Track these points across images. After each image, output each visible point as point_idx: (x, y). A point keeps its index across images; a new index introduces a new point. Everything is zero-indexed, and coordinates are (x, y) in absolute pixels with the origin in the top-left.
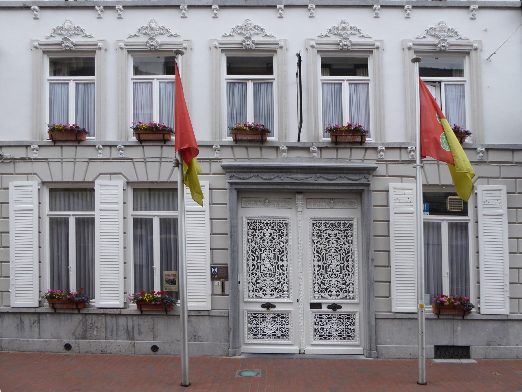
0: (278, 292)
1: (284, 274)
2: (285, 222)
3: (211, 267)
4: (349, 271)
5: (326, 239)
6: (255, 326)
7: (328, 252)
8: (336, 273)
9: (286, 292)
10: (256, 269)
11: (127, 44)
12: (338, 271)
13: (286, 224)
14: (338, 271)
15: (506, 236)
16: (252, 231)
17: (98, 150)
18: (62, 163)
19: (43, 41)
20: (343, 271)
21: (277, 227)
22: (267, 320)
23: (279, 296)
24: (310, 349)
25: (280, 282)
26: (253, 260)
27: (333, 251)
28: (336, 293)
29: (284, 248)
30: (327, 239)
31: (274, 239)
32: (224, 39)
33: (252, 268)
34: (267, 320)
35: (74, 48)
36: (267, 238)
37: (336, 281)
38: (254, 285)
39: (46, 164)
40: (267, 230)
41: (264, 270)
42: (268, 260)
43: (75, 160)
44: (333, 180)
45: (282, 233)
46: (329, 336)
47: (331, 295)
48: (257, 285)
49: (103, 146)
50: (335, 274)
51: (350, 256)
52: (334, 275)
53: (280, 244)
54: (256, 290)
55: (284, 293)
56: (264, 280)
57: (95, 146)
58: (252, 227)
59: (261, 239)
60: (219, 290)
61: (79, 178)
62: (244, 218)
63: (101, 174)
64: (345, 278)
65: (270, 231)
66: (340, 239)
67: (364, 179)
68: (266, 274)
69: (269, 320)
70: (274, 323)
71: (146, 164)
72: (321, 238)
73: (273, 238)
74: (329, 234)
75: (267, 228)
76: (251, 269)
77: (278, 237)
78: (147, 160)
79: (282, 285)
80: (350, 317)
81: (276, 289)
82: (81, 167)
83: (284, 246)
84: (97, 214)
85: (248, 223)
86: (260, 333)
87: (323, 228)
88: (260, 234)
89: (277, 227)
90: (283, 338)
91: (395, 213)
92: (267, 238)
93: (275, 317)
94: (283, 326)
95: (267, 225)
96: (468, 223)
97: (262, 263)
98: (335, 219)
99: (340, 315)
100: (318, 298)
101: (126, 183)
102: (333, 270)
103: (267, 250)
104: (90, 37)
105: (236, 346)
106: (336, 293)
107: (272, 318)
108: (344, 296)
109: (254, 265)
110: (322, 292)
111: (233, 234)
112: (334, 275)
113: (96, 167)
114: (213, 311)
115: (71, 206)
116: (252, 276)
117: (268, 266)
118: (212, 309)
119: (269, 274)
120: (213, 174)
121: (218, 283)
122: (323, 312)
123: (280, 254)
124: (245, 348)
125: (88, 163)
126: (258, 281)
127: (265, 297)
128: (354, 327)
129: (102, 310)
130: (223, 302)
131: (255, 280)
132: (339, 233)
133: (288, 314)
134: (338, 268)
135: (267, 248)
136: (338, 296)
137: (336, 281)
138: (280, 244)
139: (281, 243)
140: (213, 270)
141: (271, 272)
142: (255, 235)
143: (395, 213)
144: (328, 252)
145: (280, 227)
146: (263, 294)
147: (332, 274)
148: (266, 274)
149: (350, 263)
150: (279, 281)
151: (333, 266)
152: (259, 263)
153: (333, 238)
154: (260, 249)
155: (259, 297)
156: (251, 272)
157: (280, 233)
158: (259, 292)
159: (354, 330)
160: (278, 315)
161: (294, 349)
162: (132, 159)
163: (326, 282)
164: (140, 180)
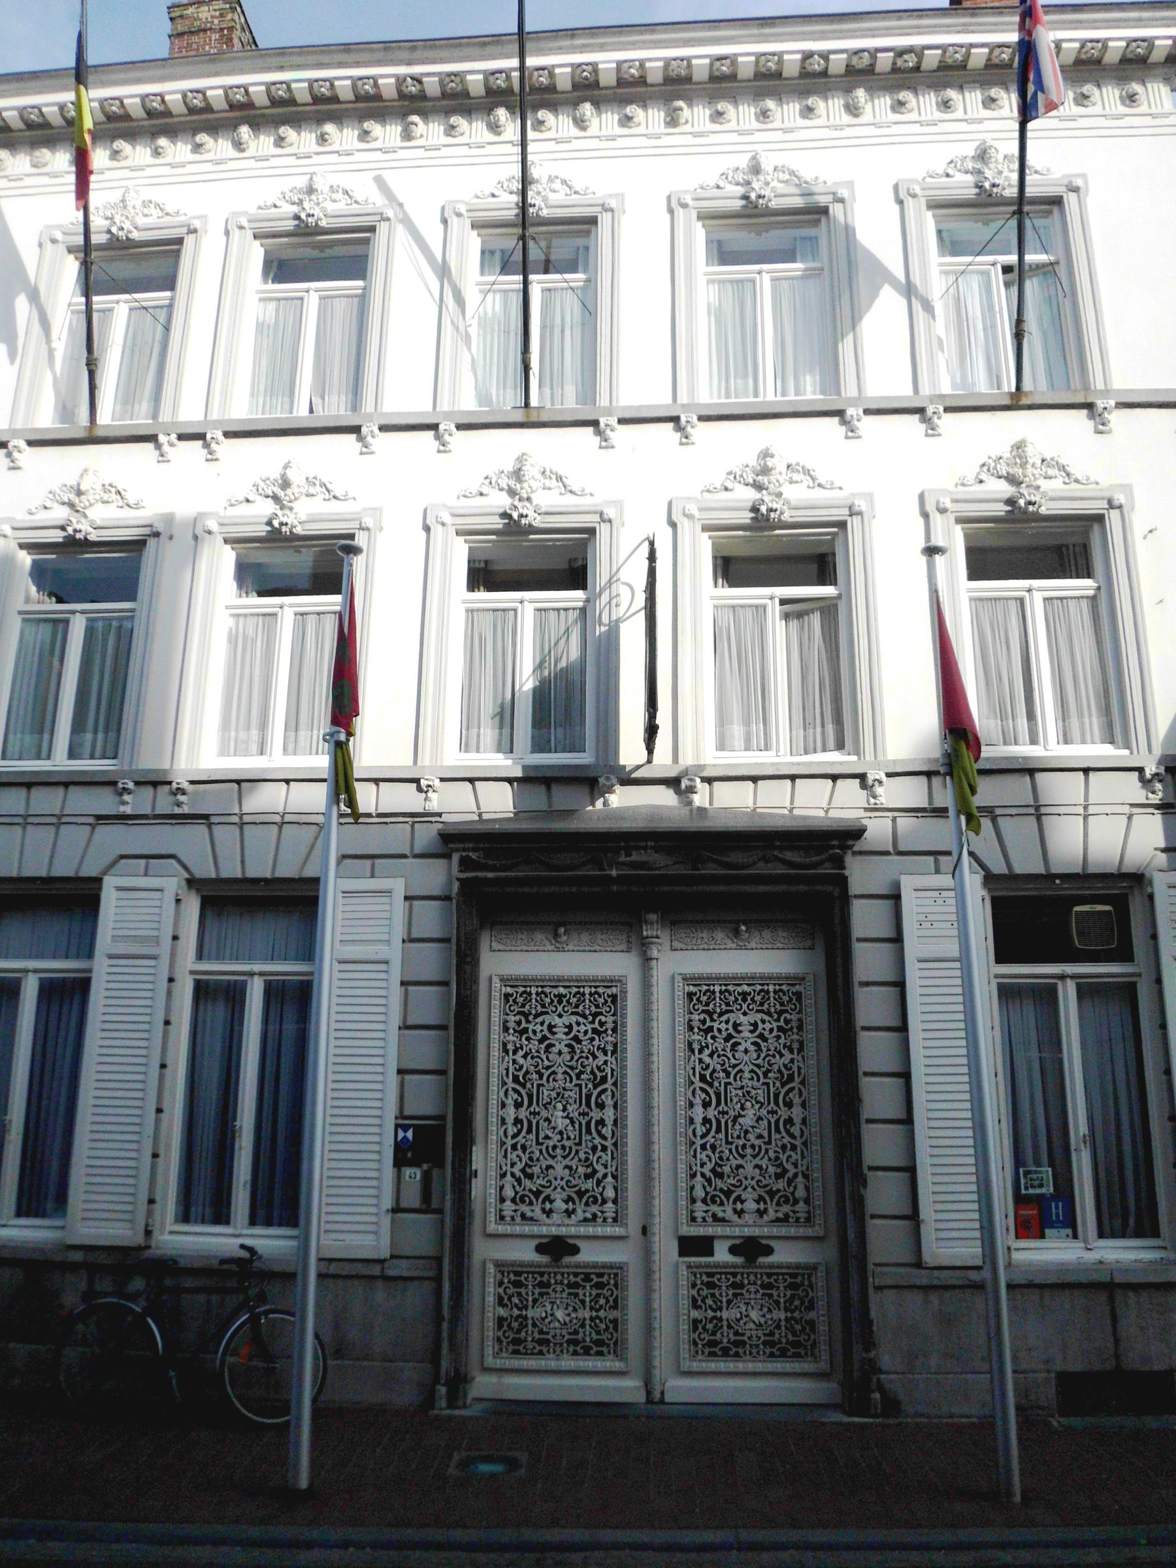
0: (587, 1204)
1: (794, 1148)
2: (609, 991)
3: (397, 1126)
4: (605, 1138)
5: (727, 1039)
6: (710, 1314)
7: (731, 1080)
8: (757, 1142)
9: (801, 1204)
10: (524, 1133)
11: (225, 522)
12: (760, 1137)
13: (614, 997)
14: (760, 1137)
15: (395, 1020)
16: (702, 1016)
17: (121, 794)
18: (24, 829)
19: (22, 518)
20: (589, 1137)
21: (587, 1007)
22: (553, 1295)
23: (589, 1216)
24: (681, 1389)
25: (595, 1171)
26: (518, 1105)
27: (747, 1075)
28: (564, 1206)
29: (795, 1069)
30: (729, 1038)
31: (579, 1041)
32: (465, 502)
33: (512, 1130)
34: (553, 1295)
35: (93, 537)
36: (561, 1040)
37: (567, 1167)
38: (519, 1181)
39: (204, 829)
40: (560, 1016)
41: (547, 1137)
42: (560, 1106)
43: (59, 821)
44: (743, 867)
45: (601, 1024)
46: (737, 1344)
47: (551, 1211)
48: (528, 1183)
49: (137, 783)
50: (753, 1147)
51: (796, 1091)
52: (749, 1151)
53: (595, 1057)
54: (522, 1197)
55: (797, 1208)
56: (549, 1167)
57: (114, 783)
58: (516, 1008)
59: (541, 1041)
60: (412, 1198)
61: (64, 868)
62: (496, 980)
63: (123, 857)
64: (783, 1158)
65: (567, 1020)
66: (765, 1040)
67: (761, 864)
68: (555, 1147)
69: (561, 1295)
70: (572, 1301)
71: (241, 829)
72: (528, 1039)
73: (576, 1039)
74: (551, 1027)
75: (560, 1009)
76: (699, 1133)
77: (589, 1035)
78: (31, 820)
79: (599, 1182)
80: (605, 1279)
81: (581, 1194)
82: (73, 837)
83: (606, 1062)
84: (101, 970)
85: (690, 995)
86: (530, 1334)
87: (717, 1005)
88: (538, 1028)
89: (587, 1007)
90: (600, 1354)
91: (111, 957)
92: (561, 1040)
93: (575, 1285)
94: (602, 1314)
95: (744, 1000)
96: (244, 983)
97: (764, 1112)
98: (751, 979)
99: (769, 1275)
100: (704, 1219)
101: (184, 883)
102: (746, 1132)
103: (560, 1076)
104: (137, 506)
105: (459, 1382)
106: (564, 1206)
107: (569, 1286)
108: (780, 1215)
109: (521, 1122)
110: (523, 1201)
111: (462, 1024)
112: (749, 1151)
113: (114, 839)
114: (394, 1261)
115: (73, 949)
116: (512, 1156)
117: (561, 1123)
118: (392, 1257)
119: (563, 1147)
120: (416, 856)
121: (413, 1174)
122: (717, 1265)
123: (595, 1087)
124: (484, 1385)
125: (93, 827)
126: (529, 1170)
127: (548, 1221)
128: (812, 1315)
129: (347, 1265)
130: (421, 1234)
131: (520, 1166)
132: (763, 1022)
133: (810, 1275)
134: (762, 1128)
135: (560, 1070)
136: (761, 1213)
137: (567, 1167)
138: (595, 1057)
139: (599, 1054)
140: (401, 1134)
141: (567, 1143)
142: (526, 1030)
143: (111, 957)
144: (731, 1080)
145: (597, 1006)
146: (543, 1210)
147: (744, 1147)
148: (555, 1147)
149: (511, 1113)
150: (589, 1170)
151: (747, 1121)
152: (535, 1114)
153: (746, 1039)
154: (724, 1071)
155: (532, 1219)
156: (510, 1142)
157: (596, 1025)
158: (531, 1203)
159: (812, 1323)
160: (587, 1278)
161: (625, 1388)
162: (206, 817)
163: (536, 1170)
164: (224, 874)
